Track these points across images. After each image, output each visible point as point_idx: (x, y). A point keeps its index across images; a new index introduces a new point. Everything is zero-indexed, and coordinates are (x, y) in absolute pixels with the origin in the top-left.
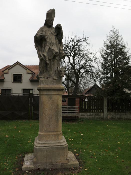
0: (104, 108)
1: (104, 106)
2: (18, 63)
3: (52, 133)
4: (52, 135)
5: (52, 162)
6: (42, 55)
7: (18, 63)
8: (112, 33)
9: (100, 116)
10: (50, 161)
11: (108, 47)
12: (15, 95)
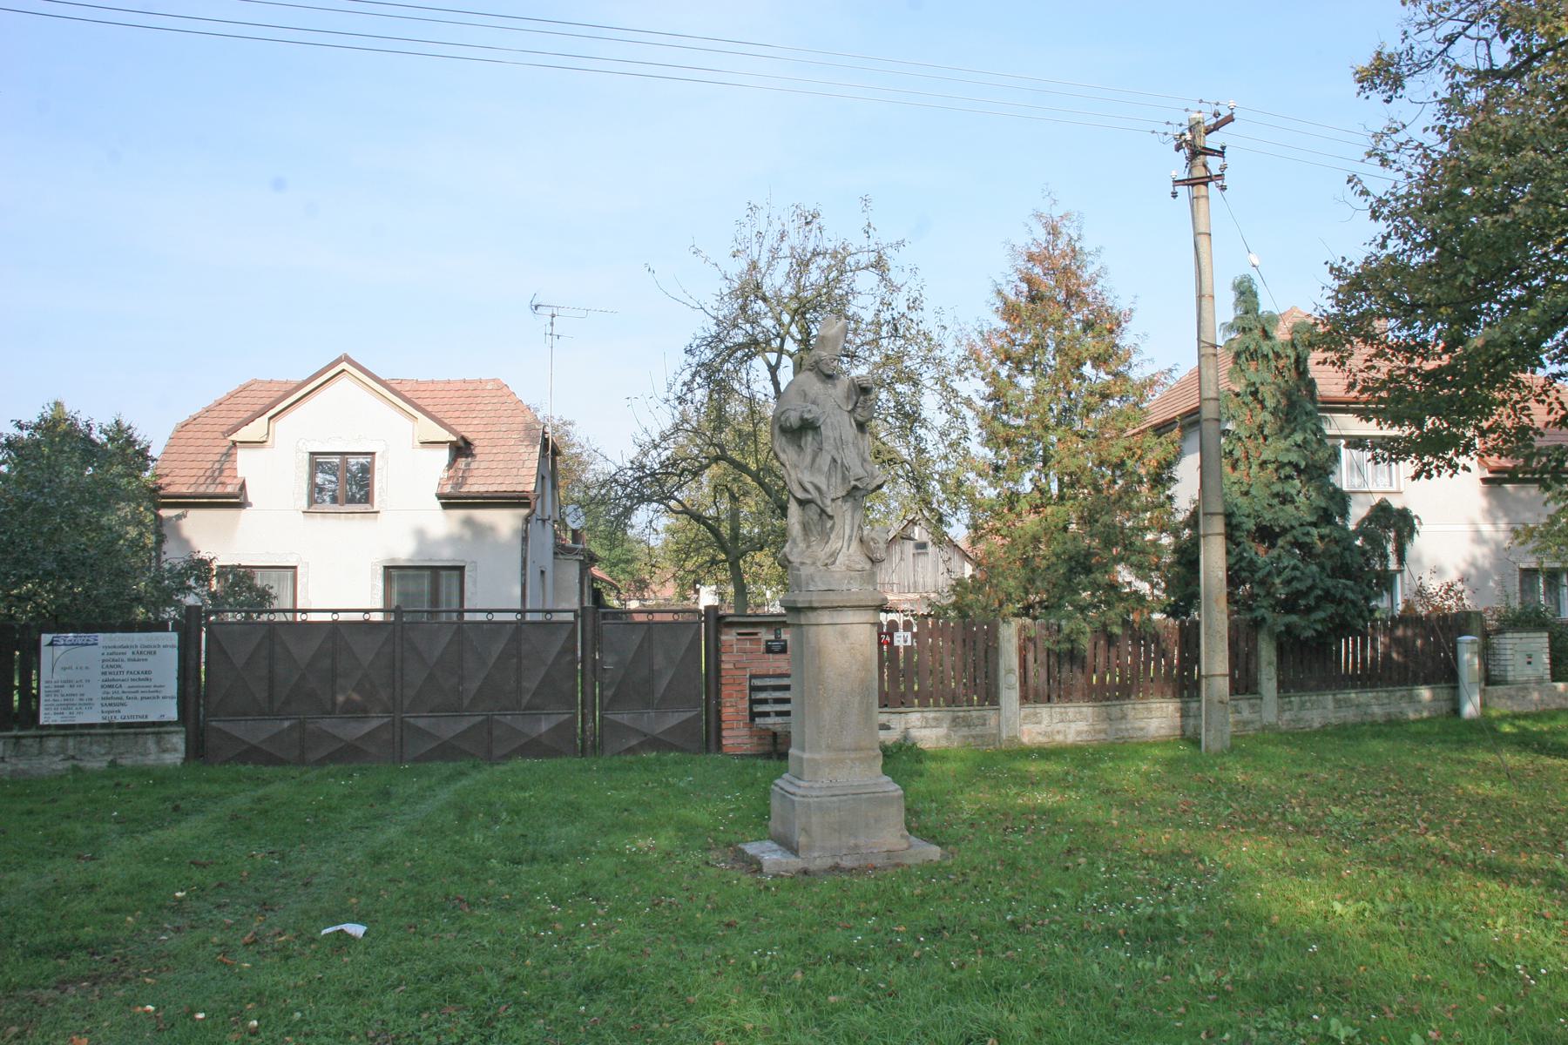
0: (1002, 685)
1: (1002, 673)
2: (344, 365)
3: (853, 755)
4: (852, 760)
5: (856, 846)
6: (809, 487)
7: (344, 365)
8: (1041, 235)
9: (978, 730)
10: (852, 842)
11: (1010, 312)
12: (313, 617)
